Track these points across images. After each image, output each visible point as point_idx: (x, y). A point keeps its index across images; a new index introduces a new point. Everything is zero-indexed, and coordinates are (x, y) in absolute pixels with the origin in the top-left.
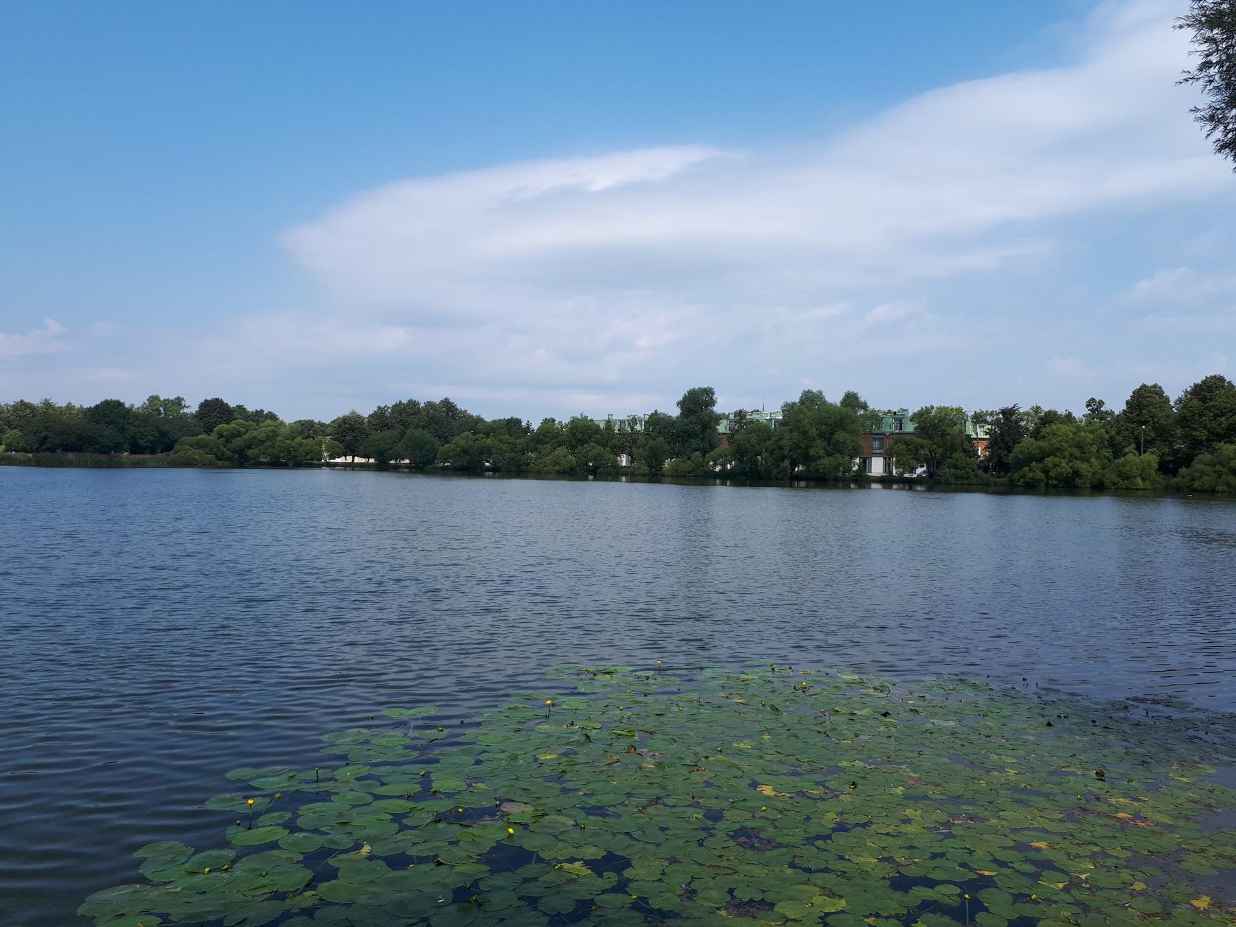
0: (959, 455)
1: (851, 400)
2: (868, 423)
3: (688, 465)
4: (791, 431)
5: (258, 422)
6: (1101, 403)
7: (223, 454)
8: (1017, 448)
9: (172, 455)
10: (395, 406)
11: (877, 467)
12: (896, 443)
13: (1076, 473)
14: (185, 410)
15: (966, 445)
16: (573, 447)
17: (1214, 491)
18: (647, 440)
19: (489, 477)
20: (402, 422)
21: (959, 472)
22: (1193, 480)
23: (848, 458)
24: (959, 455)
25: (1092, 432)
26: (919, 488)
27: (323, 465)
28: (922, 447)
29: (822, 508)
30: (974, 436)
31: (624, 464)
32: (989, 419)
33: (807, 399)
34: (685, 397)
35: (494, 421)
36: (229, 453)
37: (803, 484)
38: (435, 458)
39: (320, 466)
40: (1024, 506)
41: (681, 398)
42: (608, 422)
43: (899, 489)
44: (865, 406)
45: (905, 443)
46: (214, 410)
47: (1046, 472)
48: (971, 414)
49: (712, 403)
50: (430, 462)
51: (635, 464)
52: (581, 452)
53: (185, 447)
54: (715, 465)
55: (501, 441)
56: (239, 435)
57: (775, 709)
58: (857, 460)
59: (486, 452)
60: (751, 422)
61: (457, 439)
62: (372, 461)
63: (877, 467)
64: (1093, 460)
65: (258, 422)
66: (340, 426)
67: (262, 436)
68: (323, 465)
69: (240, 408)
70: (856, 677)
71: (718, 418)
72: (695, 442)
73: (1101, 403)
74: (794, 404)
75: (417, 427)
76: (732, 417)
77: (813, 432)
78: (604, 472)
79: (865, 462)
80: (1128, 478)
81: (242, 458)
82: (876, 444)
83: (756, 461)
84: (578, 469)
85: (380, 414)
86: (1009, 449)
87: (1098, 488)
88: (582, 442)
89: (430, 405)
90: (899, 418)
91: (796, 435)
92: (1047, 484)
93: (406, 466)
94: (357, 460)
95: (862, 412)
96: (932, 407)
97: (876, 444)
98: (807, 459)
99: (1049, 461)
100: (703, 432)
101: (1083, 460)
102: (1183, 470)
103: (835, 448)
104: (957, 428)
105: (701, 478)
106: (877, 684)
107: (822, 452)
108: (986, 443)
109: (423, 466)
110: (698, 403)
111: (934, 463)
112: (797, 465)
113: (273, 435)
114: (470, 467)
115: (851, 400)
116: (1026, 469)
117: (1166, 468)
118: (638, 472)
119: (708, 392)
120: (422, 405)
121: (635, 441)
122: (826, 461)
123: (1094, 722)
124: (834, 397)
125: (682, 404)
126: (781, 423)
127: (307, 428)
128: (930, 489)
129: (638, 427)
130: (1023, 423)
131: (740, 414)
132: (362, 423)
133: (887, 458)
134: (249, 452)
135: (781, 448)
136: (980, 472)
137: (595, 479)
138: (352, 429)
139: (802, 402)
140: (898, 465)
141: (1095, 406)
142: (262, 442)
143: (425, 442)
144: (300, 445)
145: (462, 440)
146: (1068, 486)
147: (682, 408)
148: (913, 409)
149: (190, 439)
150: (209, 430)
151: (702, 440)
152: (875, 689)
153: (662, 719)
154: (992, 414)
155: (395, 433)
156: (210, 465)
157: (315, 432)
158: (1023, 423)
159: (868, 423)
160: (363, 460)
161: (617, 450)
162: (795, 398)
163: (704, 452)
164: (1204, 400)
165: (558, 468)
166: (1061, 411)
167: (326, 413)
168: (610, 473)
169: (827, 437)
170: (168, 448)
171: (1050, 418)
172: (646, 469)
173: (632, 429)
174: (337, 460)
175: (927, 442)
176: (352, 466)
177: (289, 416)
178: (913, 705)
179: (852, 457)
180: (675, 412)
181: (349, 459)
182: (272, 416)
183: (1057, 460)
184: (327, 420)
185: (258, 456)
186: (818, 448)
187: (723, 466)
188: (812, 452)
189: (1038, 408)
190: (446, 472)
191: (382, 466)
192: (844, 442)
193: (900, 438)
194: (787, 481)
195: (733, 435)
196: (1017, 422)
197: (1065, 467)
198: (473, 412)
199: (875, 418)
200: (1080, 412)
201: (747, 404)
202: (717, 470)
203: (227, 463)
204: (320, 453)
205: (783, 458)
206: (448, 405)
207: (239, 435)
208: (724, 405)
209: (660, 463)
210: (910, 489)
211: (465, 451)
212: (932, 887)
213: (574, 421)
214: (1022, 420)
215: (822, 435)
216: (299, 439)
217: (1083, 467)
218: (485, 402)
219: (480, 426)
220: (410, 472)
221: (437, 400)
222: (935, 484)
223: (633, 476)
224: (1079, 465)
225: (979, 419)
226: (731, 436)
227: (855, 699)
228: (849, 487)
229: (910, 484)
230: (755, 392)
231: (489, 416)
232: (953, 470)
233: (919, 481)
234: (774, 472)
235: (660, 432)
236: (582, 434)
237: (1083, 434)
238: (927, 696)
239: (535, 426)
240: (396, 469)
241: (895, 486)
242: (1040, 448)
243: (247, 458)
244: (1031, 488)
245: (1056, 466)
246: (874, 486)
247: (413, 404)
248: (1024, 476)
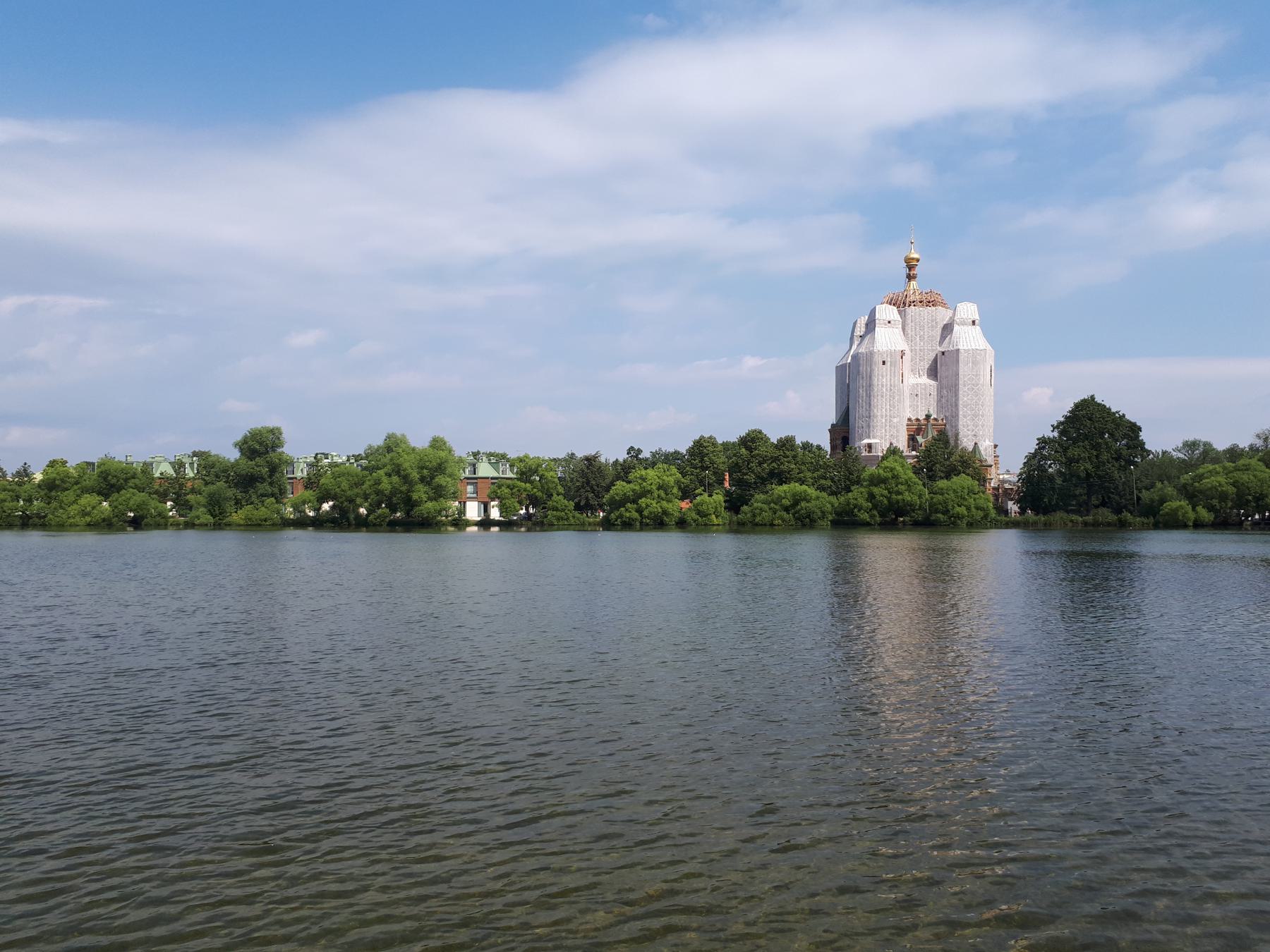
1: (437, 444)
13: (665, 512)
17: (772, 525)
21: (558, 514)
22: (754, 516)
29: (410, 548)
41: (239, 438)
47: (640, 511)
68: (229, 525)
72: (264, 487)
73: (639, 451)
77: (415, 475)
80: (706, 516)
91: (395, 479)
92: (641, 523)
98: (410, 504)
99: (643, 501)
100: (270, 476)
101: (669, 501)
102: (745, 508)
103: (439, 493)
107: (424, 497)
110: (261, 446)
115: (437, 444)
117: (734, 504)
119: (275, 433)
135: (378, 493)
139: (691, 452)
147: (241, 450)
151: (271, 484)
164: (749, 449)
165: (88, 519)
180: (232, 455)
186: (420, 492)
188: (415, 496)
212: (253, 903)
215: (422, 479)
220: (1261, 529)
230: (326, 434)
242: (633, 490)
245: (647, 506)
248: (621, 516)
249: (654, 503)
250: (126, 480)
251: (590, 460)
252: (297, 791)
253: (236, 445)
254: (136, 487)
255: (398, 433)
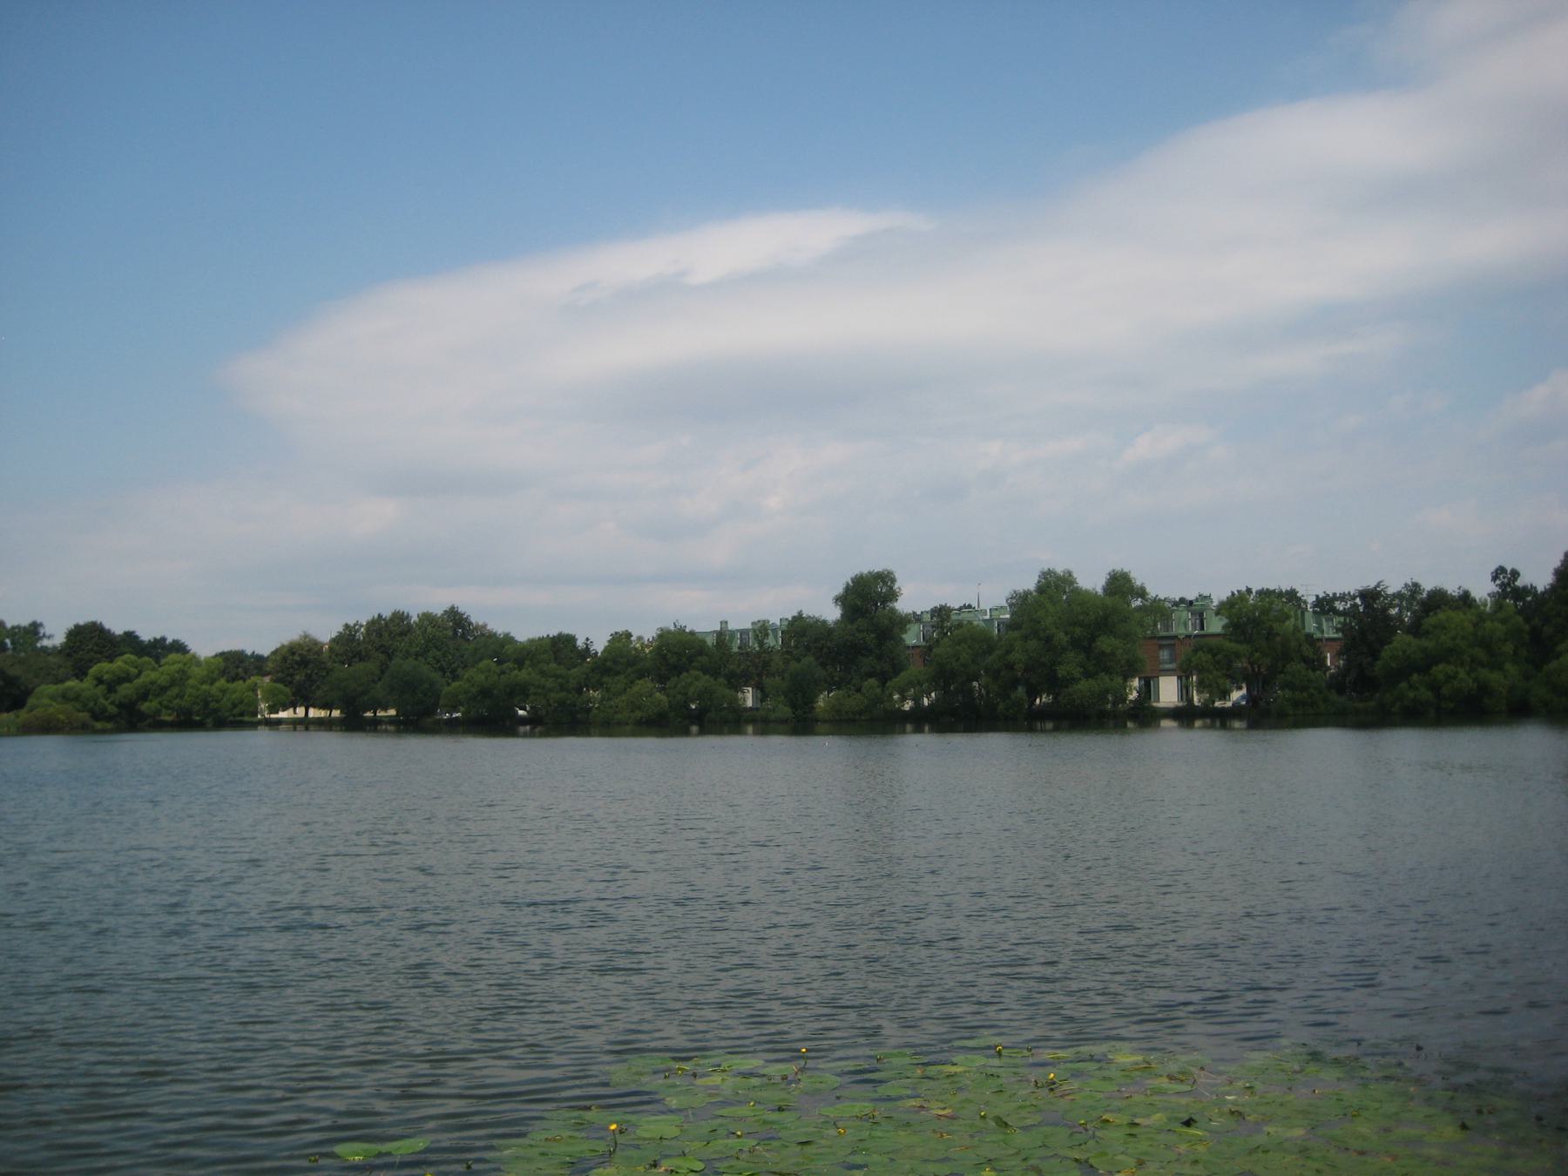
0: (1296, 667)
1: (1120, 584)
2: (1149, 620)
3: (854, 702)
4: (1025, 638)
5: (157, 659)
6: (1515, 574)
7: (104, 710)
8: (1386, 652)
9: (23, 715)
10: (372, 623)
11: (1168, 692)
12: (1195, 651)
13: (1484, 689)
14: (45, 643)
15: (1307, 651)
16: (662, 679)
18: (787, 662)
19: (525, 735)
20: (383, 649)
23: (1120, 680)
24: (1296, 667)
25: (1504, 621)
26: (1237, 724)
27: (259, 723)
28: (1238, 655)
30: (1318, 635)
31: (749, 703)
32: (1340, 606)
33: (1048, 585)
34: (847, 588)
35: (531, 641)
36: (112, 709)
37: (1049, 725)
38: (436, 705)
39: (254, 725)
40: (1406, 747)
41: (840, 590)
42: (720, 635)
43: (1205, 727)
44: (1142, 593)
45: (1210, 650)
46: (91, 642)
47: (1435, 687)
48: (1311, 599)
49: (892, 595)
50: (430, 711)
51: (769, 704)
52: (680, 687)
53: (45, 698)
54: (903, 699)
55: (542, 673)
56: (127, 678)
57: (1002, 1124)
58: (1136, 683)
59: (519, 692)
60: (960, 625)
61: (470, 672)
62: (336, 713)
63: (1168, 692)
64: (1508, 666)
65: (157, 659)
66: (285, 659)
67: (163, 680)
68: (259, 723)
69: (130, 637)
70: (1140, 1058)
71: (903, 622)
73: (1515, 574)
74: (1027, 594)
75: (407, 655)
76: (927, 618)
77: (1061, 637)
78: (714, 718)
79: (1147, 685)
81: (131, 717)
82: (1164, 655)
83: (971, 690)
84: (672, 714)
85: (347, 638)
86: (1375, 655)
87: (1518, 711)
88: (678, 669)
89: (427, 618)
90: (1197, 608)
93: (391, 721)
94: (313, 713)
95: (1138, 603)
96: (1249, 591)
97: (1164, 655)
98: (1054, 683)
99: (1440, 670)
103: (1099, 664)
104: (1290, 623)
105: (876, 722)
106: (1173, 1068)
107: (1077, 672)
108: (1337, 646)
109: (419, 718)
110: (868, 597)
111: (1257, 681)
112: (1038, 694)
113: (180, 679)
114: (492, 717)
115: (1120, 584)
116: (1404, 685)
118: (773, 716)
119: (885, 578)
120: (415, 619)
121: (766, 664)
122: (1084, 686)
123: (1539, 1119)
124: (1092, 581)
125: (841, 600)
126: (1011, 626)
127: (236, 664)
128: (1254, 725)
129: (770, 641)
130: (1394, 611)
131: (941, 613)
132: (320, 652)
133: (1183, 674)
134: (145, 707)
135: (1010, 667)
136: (1334, 696)
137: (703, 732)
138: (304, 663)
139: (1041, 589)
140: (1201, 686)
141: (1505, 578)
142: (164, 689)
143: (417, 679)
144: (224, 691)
145: (479, 674)
146: (1470, 709)
148: (1220, 594)
149: (52, 689)
150: (81, 673)
151: (879, 658)
152: (1171, 1078)
153: (809, 1150)
154: (1342, 598)
155: (371, 666)
156: (84, 729)
157: (246, 670)
158: (1394, 611)
159: (1149, 620)
160: (322, 713)
161: (737, 681)
162: (1029, 583)
163: (884, 678)
165: (638, 714)
166: (1452, 589)
167: (263, 641)
168: (730, 721)
169: (1084, 645)
170: (18, 703)
171: (1438, 599)
172: (785, 711)
173: (761, 644)
174: (282, 715)
175: (1243, 648)
176: (306, 724)
177: (205, 646)
178: (1234, 1103)
179: (1127, 677)
181: (301, 712)
182: (179, 647)
183: (1450, 669)
184: (265, 650)
185: (158, 712)
186: (1070, 665)
187: (917, 700)
188: (1062, 671)
189: (1416, 585)
190: (452, 728)
191: (353, 723)
192: (1113, 654)
193: (1202, 643)
194: (1023, 721)
195: (930, 648)
196: (1385, 610)
197: (1465, 679)
198: (498, 627)
199: (1159, 610)
200: (1483, 589)
201: (953, 596)
202: (908, 706)
203: (109, 726)
204: (255, 703)
205: (1014, 683)
206: (456, 619)
207: (127, 678)
208: (913, 599)
209: (809, 702)
210: (1224, 726)
211: (485, 693)
213: (664, 635)
214: (1392, 606)
216: (222, 682)
217: (1494, 678)
218: (517, 612)
219: (509, 649)
221: (438, 610)
222: (1261, 715)
223: (764, 724)
224: (1484, 673)
225: (1325, 605)
226: (927, 650)
227: (1136, 1098)
228: (1125, 726)
229: (1220, 719)
230: (960, 572)
231: (524, 632)
232: (1288, 693)
233: (1236, 712)
234: (1001, 707)
235: (808, 648)
236: (678, 655)
237: (1488, 624)
238: (1258, 1086)
239: (599, 645)
240: (373, 726)
241: (1198, 723)
243: (142, 716)
244: (1413, 716)
245: (1450, 678)
246: (1166, 723)
247: (399, 617)
249: (1462, 674)
250: (691, 659)
251: (1370, 596)
252: (308, 910)
253: (1070, 574)
254: (705, 670)
255: (1059, 570)
